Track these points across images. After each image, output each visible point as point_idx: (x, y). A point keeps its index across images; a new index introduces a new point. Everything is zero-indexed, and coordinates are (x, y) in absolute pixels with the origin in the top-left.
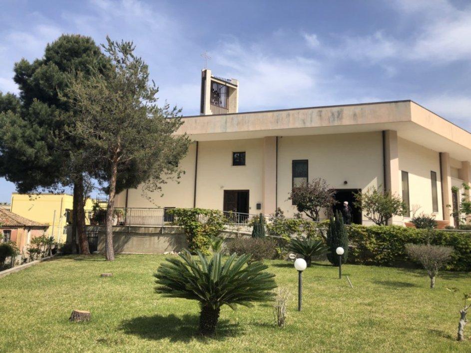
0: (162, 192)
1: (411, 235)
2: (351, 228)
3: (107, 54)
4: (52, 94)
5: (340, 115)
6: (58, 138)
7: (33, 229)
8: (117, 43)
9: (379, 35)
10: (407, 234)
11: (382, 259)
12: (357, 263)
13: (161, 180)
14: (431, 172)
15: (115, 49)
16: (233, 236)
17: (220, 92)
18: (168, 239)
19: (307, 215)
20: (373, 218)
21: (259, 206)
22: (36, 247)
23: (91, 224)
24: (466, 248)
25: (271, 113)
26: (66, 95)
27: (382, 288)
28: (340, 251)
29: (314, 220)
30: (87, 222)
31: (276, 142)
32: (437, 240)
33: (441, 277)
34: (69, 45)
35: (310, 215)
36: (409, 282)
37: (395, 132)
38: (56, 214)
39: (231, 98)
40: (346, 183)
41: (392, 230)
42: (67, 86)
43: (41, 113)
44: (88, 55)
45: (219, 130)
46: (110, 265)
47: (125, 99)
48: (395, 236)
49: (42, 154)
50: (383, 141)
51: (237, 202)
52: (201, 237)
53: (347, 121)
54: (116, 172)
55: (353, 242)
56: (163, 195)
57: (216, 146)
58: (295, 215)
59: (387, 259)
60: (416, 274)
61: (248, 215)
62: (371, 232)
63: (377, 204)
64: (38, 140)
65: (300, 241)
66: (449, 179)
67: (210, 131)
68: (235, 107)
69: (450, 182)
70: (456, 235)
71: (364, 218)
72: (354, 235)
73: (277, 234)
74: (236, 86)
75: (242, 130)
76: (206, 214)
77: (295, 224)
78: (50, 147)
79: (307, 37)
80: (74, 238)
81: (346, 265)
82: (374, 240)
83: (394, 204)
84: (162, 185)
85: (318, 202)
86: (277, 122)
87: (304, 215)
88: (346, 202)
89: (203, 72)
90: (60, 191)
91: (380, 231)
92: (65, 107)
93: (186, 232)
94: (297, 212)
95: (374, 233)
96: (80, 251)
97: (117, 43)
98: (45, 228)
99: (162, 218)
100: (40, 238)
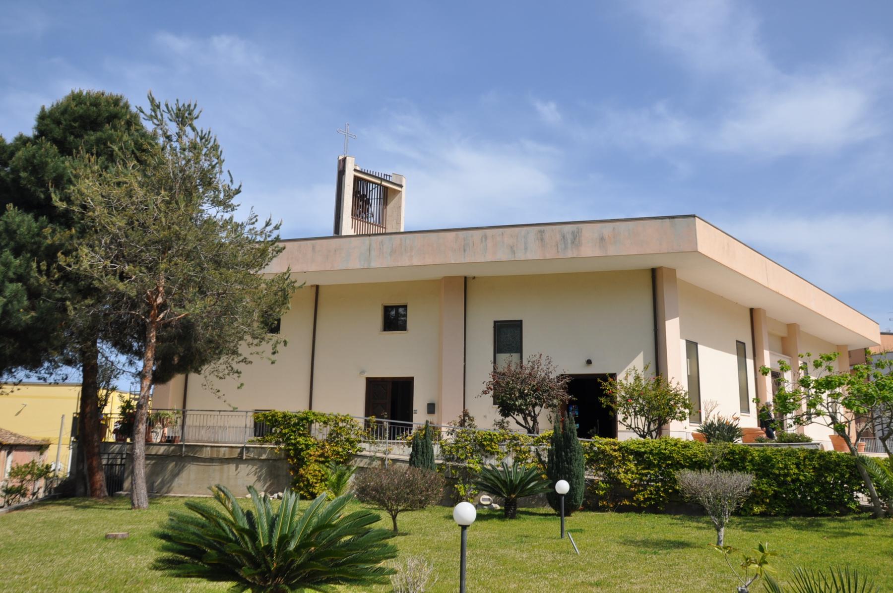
0: (241, 380)
1: (695, 455)
2: (592, 445)
3: (149, 126)
4: (42, 196)
5: (576, 239)
6: (45, 277)
7: (17, 450)
8: (167, 106)
9: (661, 108)
10: (689, 453)
11: (646, 500)
12: (603, 509)
13: (241, 358)
14: (737, 341)
15: (162, 115)
16: (376, 464)
17: (370, 197)
18: (254, 469)
19: (518, 423)
20: (633, 426)
21: (431, 408)
22: (18, 485)
23: (117, 439)
24: (786, 475)
25: (453, 234)
26: (67, 199)
27: (632, 552)
28: (563, 486)
29: (530, 432)
30: (111, 438)
31: (464, 287)
32: (735, 462)
33: (742, 528)
34: (80, 110)
35: (523, 423)
36: (684, 538)
37: (673, 271)
38: (65, 421)
39: (389, 207)
40: (589, 362)
41: (663, 447)
42: (70, 182)
43: (18, 232)
44: (114, 128)
45: (355, 264)
46: (136, 516)
47: (174, 205)
48: (670, 458)
49: (16, 307)
50: (656, 282)
51: (390, 399)
52: (316, 467)
53: (589, 250)
54: (153, 341)
55: (597, 470)
56: (242, 385)
57: (352, 293)
58: (496, 424)
59: (654, 499)
60: (700, 525)
61: (411, 425)
62: (626, 452)
63: (641, 401)
64: (11, 281)
65: (497, 471)
66: (766, 353)
67: (340, 265)
68: (399, 223)
69: (768, 360)
70: (768, 453)
71: (620, 427)
72: (597, 459)
73: (458, 458)
74: (401, 186)
75: (400, 264)
76: (325, 423)
77: (491, 440)
78: (34, 294)
79: (539, 106)
80: (81, 467)
81: (583, 513)
82: (632, 466)
83: (670, 400)
84: (241, 367)
85: (537, 398)
86: (465, 251)
87: (514, 424)
88: (589, 401)
89: (339, 161)
90: (59, 378)
91: (643, 450)
92: (65, 220)
93: (288, 456)
94: (499, 418)
95: (632, 452)
96: (89, 492)
97: (167, 106)
98: (41, 448)
99: (250, 431)
100: (27, 466)
